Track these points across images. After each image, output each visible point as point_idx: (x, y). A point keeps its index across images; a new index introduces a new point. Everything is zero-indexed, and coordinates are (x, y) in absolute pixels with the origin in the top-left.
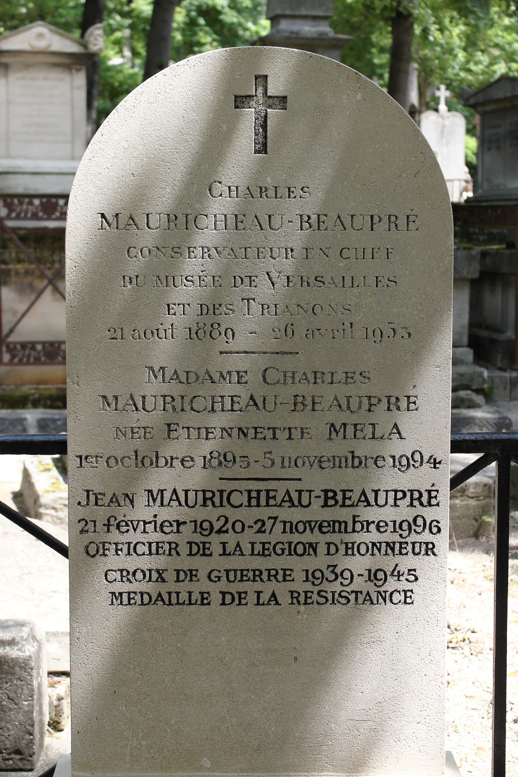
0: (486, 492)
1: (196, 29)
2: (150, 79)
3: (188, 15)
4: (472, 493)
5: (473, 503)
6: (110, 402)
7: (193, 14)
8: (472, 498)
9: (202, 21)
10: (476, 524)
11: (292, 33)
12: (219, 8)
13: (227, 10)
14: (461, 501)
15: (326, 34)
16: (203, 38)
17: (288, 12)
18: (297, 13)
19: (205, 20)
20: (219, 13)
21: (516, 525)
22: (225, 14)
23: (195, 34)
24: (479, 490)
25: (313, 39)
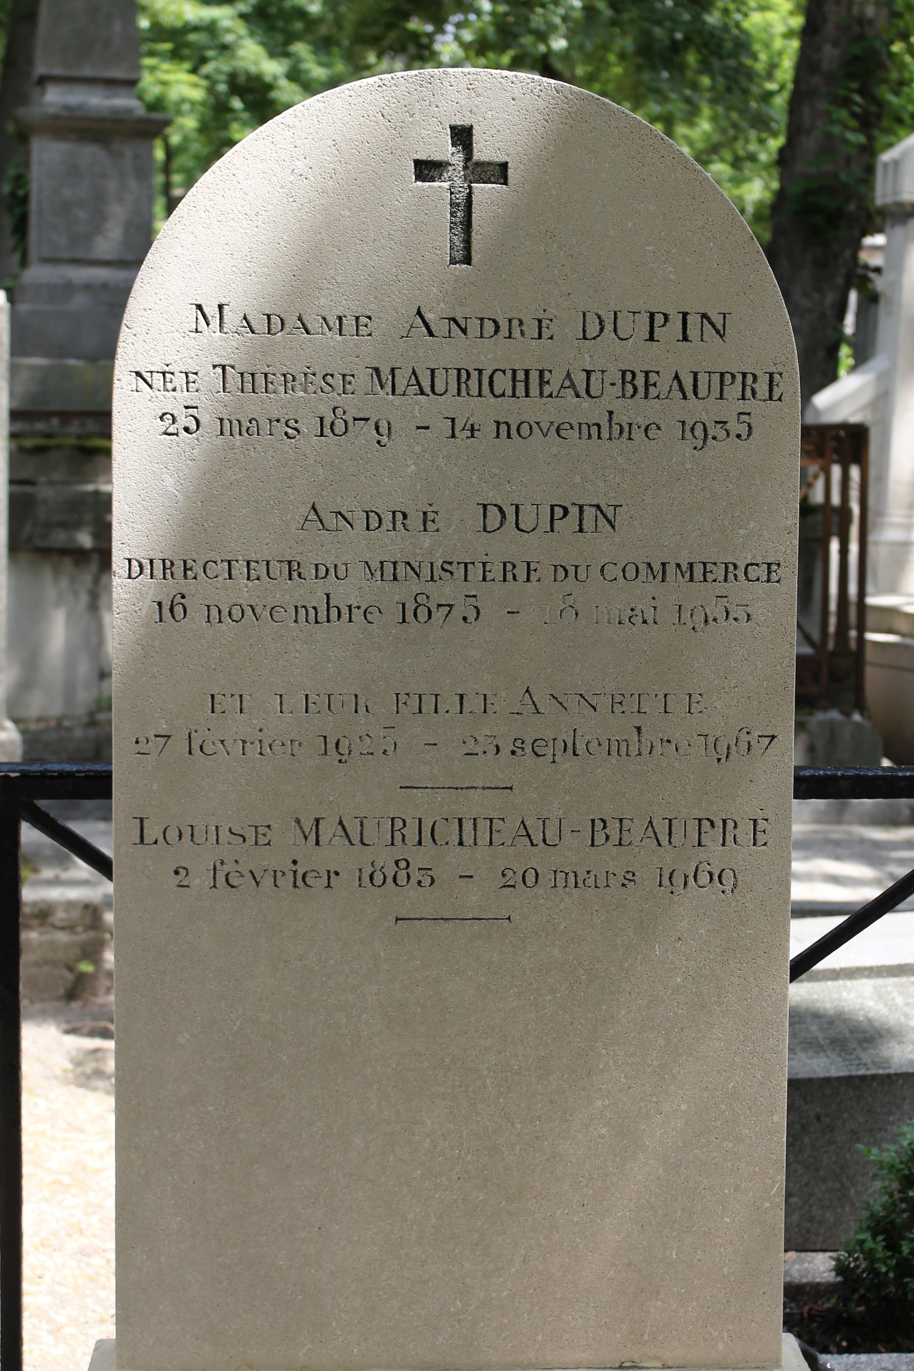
0: (88, 920)
1: (229, 116)
2: (175, 212)
3: (211, 90)
4: (61, 920)
5: (63, 937)
6: (307, 831)
7: (222, 88)
8: (62, 928)
9: (237, 103)
10: (70, 976)
11: (67, 108)
12: (268, 79)
13: (283, 83)
14: (41, 934)
15: (129, 111)
16: (238, 132)
17: (58, 71)
18: (77, 73)
19: (243, 101)
20: (269, 87)
21: (911, 1000)
22: (279, 88)
23: (225, 127)
24: (75, 914)
25: (102, 120)
